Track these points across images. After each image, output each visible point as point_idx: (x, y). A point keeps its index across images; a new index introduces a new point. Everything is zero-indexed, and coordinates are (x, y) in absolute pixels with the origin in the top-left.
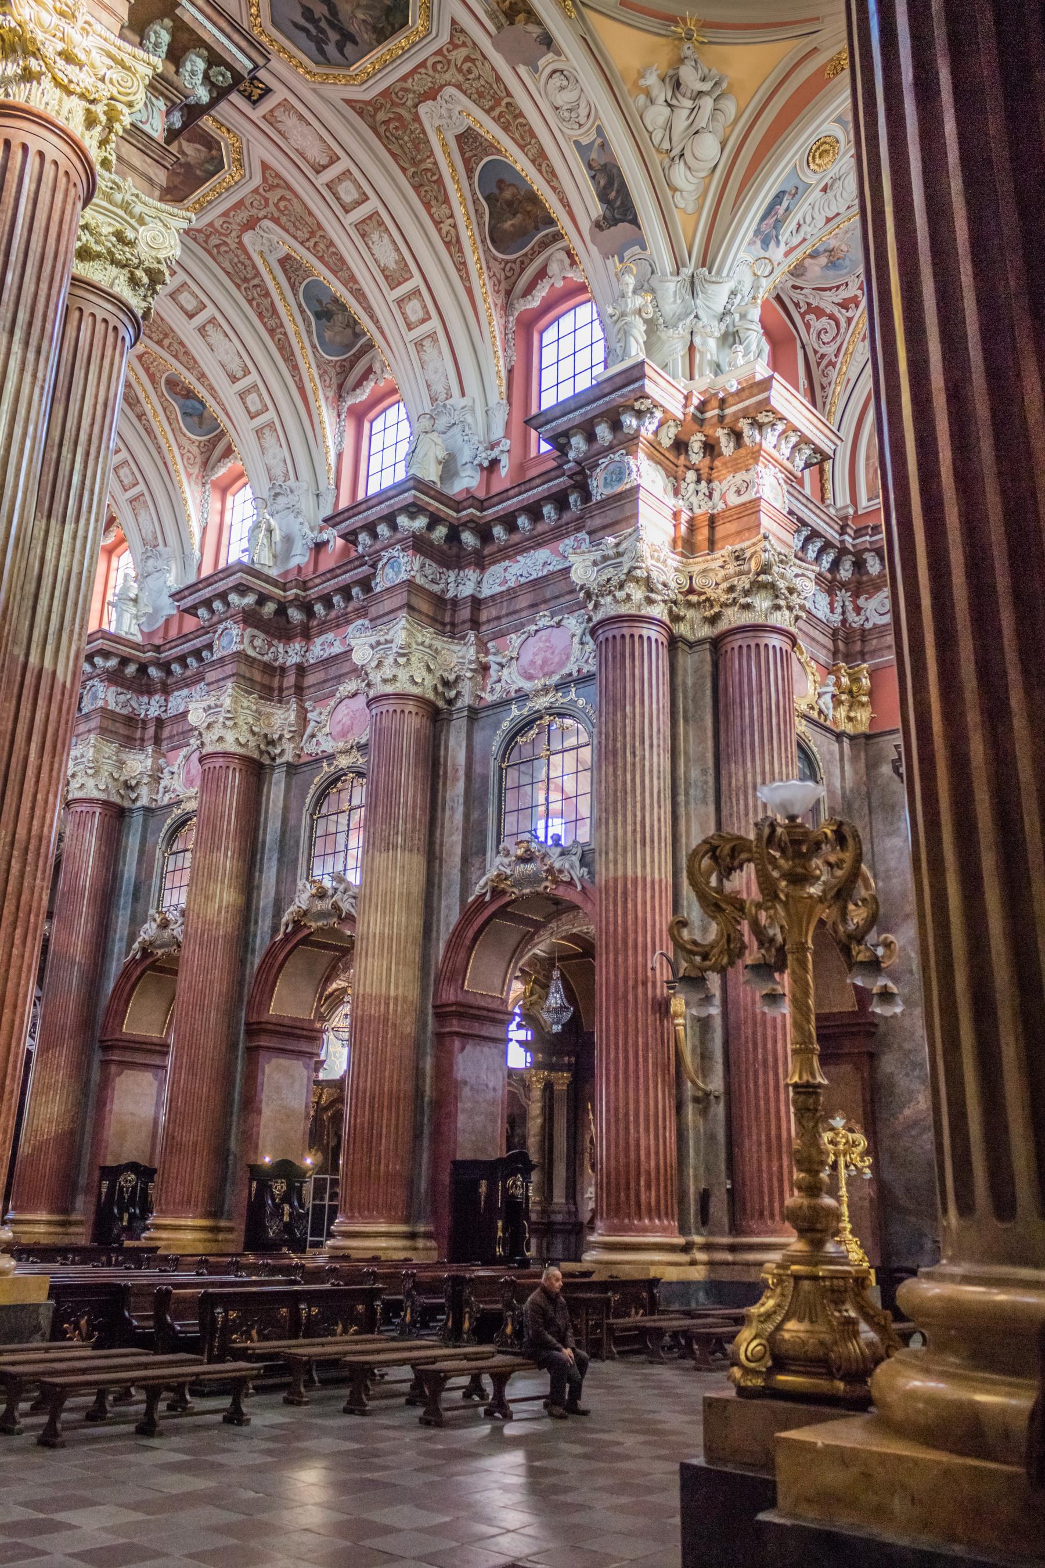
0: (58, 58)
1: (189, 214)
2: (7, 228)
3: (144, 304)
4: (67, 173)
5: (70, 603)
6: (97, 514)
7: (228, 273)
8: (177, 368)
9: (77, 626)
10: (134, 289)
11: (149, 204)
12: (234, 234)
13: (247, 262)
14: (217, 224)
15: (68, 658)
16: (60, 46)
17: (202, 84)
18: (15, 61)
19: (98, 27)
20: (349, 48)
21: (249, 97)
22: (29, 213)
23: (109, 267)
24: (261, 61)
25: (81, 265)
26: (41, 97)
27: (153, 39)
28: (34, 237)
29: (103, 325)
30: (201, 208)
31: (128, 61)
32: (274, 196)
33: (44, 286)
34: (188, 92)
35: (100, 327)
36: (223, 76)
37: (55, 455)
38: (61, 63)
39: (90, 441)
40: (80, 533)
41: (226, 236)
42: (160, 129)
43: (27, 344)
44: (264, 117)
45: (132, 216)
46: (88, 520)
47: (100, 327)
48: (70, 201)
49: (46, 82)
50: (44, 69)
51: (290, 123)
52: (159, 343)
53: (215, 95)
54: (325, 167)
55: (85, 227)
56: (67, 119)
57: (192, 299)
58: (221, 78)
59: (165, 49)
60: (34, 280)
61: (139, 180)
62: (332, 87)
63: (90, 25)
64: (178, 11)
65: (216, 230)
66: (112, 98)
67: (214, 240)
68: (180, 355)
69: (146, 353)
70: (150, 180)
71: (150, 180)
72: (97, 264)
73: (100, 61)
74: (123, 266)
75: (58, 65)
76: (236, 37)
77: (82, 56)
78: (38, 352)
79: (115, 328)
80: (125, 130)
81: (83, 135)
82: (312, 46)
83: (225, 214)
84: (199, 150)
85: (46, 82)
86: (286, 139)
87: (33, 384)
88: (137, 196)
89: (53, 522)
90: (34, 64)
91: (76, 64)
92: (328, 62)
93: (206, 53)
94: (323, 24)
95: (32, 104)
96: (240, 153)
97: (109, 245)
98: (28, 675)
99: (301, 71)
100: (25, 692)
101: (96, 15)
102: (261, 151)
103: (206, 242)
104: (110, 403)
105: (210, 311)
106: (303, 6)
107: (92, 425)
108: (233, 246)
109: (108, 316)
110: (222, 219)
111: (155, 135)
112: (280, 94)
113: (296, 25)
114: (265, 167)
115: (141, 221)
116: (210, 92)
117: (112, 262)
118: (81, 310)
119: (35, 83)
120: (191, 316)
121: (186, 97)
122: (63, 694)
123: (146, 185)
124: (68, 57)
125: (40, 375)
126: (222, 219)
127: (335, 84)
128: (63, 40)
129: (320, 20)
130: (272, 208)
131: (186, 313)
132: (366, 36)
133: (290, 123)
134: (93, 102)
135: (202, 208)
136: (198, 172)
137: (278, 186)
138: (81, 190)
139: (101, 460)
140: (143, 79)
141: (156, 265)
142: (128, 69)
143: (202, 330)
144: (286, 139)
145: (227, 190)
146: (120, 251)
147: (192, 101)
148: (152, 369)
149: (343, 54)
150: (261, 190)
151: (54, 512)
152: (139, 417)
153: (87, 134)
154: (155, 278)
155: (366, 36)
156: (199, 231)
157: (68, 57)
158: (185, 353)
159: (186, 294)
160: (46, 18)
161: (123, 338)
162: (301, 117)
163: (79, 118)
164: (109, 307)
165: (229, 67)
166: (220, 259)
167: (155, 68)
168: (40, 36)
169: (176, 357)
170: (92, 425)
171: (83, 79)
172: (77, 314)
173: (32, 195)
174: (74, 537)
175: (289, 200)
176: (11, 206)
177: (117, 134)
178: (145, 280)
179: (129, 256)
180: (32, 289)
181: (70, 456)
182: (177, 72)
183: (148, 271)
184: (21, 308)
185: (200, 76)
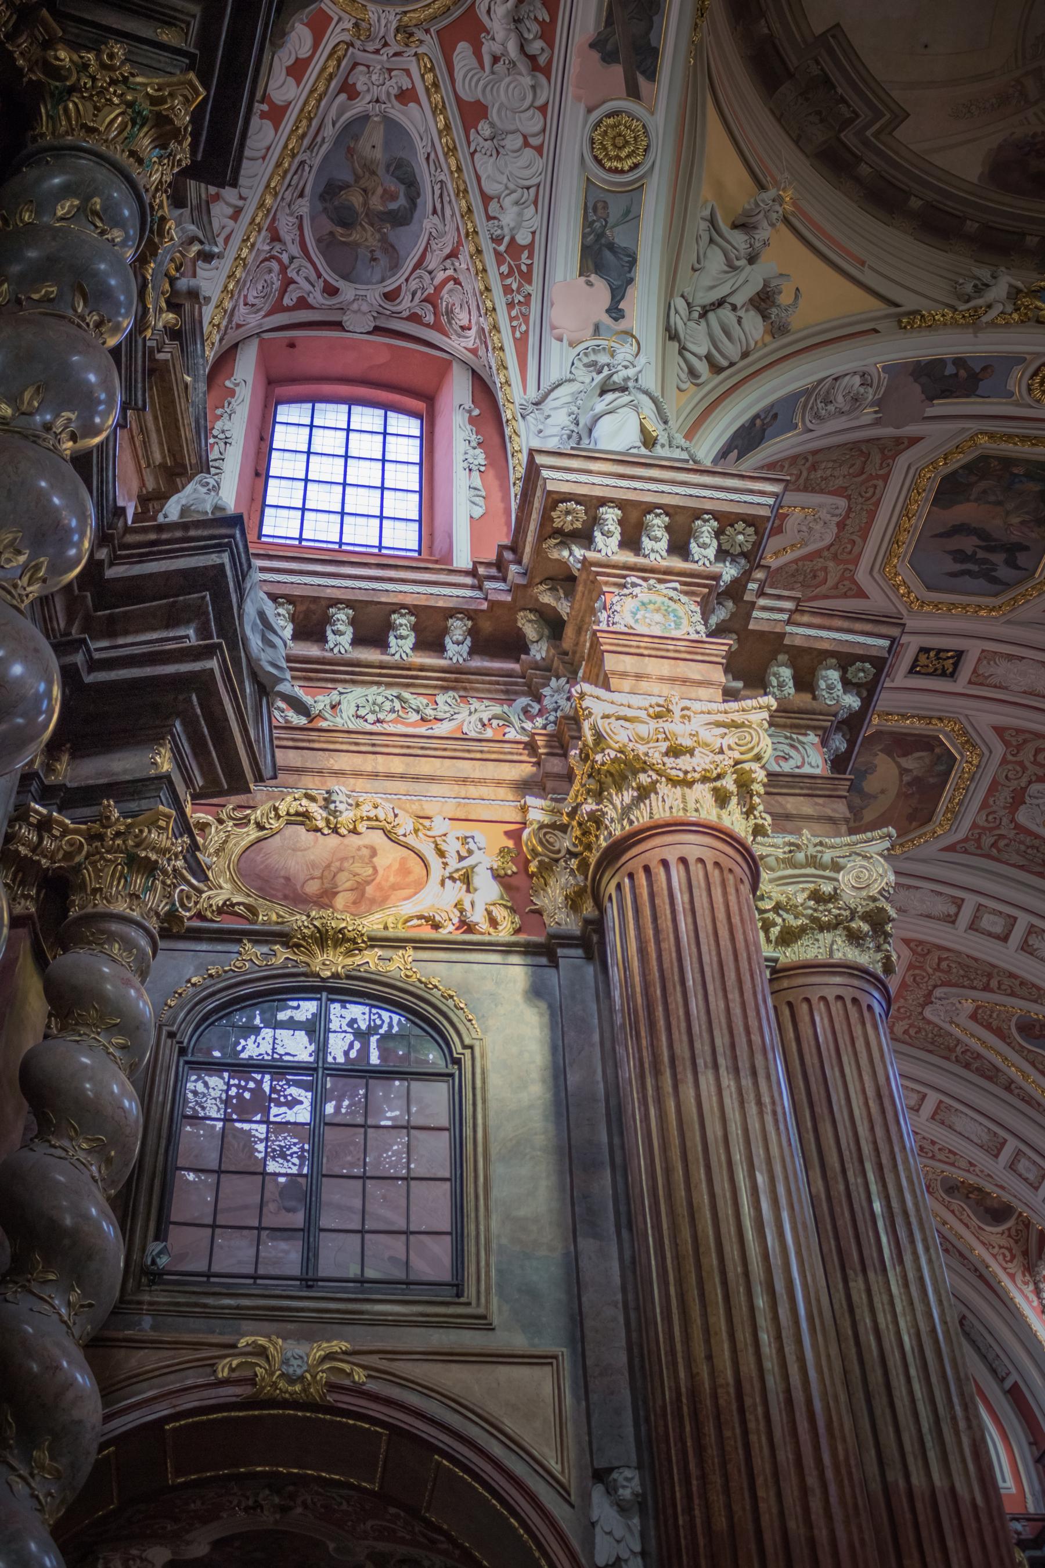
0: (665, 759)
1: (885, 830)
2: (674, 955)
3: (879, 956)
4: (717, 864)
5: (934, 1379)
6: (925, 1240)
7: (1021, 867)
8: (1019, 1006)
9: (958, 1408)
10: (858, 945)
11: (837, 845)
12: (1005, 821)
13: (1037, 842)
14: (981, 822)
15: (964, 1461)
16: (664, 746)
17: (845, 692)
18: (629, 786)
19: (697, 706)
20: (1022, 558)
21: (944, 674)
22: (691, 927)
23: (820, 936)
24: (895, 632)
25: (788, 952)
26: (668, 802)
27: (775, 682)
28: (704, 948)
29: (839, 1004)
30: (955, 814)
31: (738, 718)
32: (1027, 755)
33: (734, 996)
34: (833, 709)
35: (836, 1008)
36: (863, 670)
37: (842, 1187)
38: (670, 761)
39: (877, 1150)
40: (911, 1275)
41: (998, 827)
42: (820, 762)
43: (737, 1070)
44: (970, 682)
45: (824, 867)
46: (915, 1253)
47: (836, 1008)
48: (731, 890)
49: (663, 788)
50: (655, 777)
51: (1001, 670)
52: (986, 988)
53: (865, 694)
54: (957, 915)
55: (777, 908)
56: (697, 810)
57: (996, 919)
58: (862, 674)
59: (791, 684)
60: (720, 994)
61: (817, 827)
62: (1027, 606)
63: (688, 709)
64: (787, 641)
65: (983, 828)
66: (737, 763)
67: (987, 840)
68: (1017, 990)
69: (978, 1008)
70: (831, 820)
71: (831, 820)
72: (805, 941)
73: (712, 736)
74: (835, 927)
75: (668, 765)
76: (858, 626)
77: (687, 742)
78: (754, 1073)
79: (855, 1001)
80: (764, 785)
81: (719, 817)
82: (982, 581)
83: (984, 805)
84: (920, 758)
85: (663, 788)
86: (1006, 688)
87: (761, 1113)
88: (821, 844)
89: (871, 1275)
90: (644, 779)
91: (684, 753)
92: (1008, 586)
93: (834, 661)
94: (981, 554)
95: (656, 817)
96: (965, 733)
97: (810, 912)
98: (919, 1505)
99: (983, 613)
100: (924, 1534)
101: (693, 695)
102: (986, 718)
103: (979, 847)
104: (885, 1092)
105: (1023, 920)
106: (950, 553)
107: (872, 1129)
108: (1011, 834)
109: (840, 991)
110: (984, 813)
111: (817, 771)
112: (974, 649)
113: (954, 575)
114: (999, 730)
115: (837, 867)
116: (859, 694)
117: (821, 929)
118: (807, 1000)
119: (653, 795)
120: (1004, 938)
121: (835, 715)
122: (978, 1519)
123: (828, 827)
124: (675, 752)
125: (766, 1100)
126: (984, 813)
127: (1028, 601)
128: (666, 739)
129: (975, 553)
130: (1032, 769)
131: (997, 937)
132: (1034, 535)
133: (1001, 670)
134: (719, 777)
135: (956, 815)
136: (932, 780)
137: (1025, 741)
138: (741, 871)
139: (901, 1167)
140: (761, 725)
141: (872, 905)
142: (742, 725)
143: (1025, 947)
144: (1006, 688)
145: (972, 779)
146: (826, 914)
147: (843, 715)
148: (995, 1024)
149: (1019, 568)
150: (1010, 757)
151: (868, 1262)
152: (1008, 1088)
153: (724, 813)
154: (877, 920)
155: (1034, 535)
156: (966, 840)
157: (675, 752)
158: (1022, 984)
159: (986, 916)
160: (643, 730)
161: (870, 1008)
162: (1010, 657)
163: (709, 800)
164: (838, 980)
165: (863, 658)
166: (1005, 856)
167: (768, 707)
168: (641, 749)
169: (1013, 994)
170: (872, 1129)
171: (700, 762)
172: (805, 1006)
173: (687, 906)
174: (906, 1285)
175: (947, 959)
176: (671, 930)
177: (759, 795)
178: (866, 927)
179: (835, 911)
180: (722, 1005)
181: (860, 1180)
182: (814, 698)
183: (866, 917)
184: (717, 1033)
185: (839, 686)
